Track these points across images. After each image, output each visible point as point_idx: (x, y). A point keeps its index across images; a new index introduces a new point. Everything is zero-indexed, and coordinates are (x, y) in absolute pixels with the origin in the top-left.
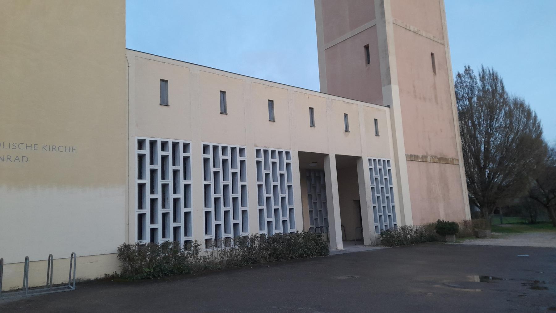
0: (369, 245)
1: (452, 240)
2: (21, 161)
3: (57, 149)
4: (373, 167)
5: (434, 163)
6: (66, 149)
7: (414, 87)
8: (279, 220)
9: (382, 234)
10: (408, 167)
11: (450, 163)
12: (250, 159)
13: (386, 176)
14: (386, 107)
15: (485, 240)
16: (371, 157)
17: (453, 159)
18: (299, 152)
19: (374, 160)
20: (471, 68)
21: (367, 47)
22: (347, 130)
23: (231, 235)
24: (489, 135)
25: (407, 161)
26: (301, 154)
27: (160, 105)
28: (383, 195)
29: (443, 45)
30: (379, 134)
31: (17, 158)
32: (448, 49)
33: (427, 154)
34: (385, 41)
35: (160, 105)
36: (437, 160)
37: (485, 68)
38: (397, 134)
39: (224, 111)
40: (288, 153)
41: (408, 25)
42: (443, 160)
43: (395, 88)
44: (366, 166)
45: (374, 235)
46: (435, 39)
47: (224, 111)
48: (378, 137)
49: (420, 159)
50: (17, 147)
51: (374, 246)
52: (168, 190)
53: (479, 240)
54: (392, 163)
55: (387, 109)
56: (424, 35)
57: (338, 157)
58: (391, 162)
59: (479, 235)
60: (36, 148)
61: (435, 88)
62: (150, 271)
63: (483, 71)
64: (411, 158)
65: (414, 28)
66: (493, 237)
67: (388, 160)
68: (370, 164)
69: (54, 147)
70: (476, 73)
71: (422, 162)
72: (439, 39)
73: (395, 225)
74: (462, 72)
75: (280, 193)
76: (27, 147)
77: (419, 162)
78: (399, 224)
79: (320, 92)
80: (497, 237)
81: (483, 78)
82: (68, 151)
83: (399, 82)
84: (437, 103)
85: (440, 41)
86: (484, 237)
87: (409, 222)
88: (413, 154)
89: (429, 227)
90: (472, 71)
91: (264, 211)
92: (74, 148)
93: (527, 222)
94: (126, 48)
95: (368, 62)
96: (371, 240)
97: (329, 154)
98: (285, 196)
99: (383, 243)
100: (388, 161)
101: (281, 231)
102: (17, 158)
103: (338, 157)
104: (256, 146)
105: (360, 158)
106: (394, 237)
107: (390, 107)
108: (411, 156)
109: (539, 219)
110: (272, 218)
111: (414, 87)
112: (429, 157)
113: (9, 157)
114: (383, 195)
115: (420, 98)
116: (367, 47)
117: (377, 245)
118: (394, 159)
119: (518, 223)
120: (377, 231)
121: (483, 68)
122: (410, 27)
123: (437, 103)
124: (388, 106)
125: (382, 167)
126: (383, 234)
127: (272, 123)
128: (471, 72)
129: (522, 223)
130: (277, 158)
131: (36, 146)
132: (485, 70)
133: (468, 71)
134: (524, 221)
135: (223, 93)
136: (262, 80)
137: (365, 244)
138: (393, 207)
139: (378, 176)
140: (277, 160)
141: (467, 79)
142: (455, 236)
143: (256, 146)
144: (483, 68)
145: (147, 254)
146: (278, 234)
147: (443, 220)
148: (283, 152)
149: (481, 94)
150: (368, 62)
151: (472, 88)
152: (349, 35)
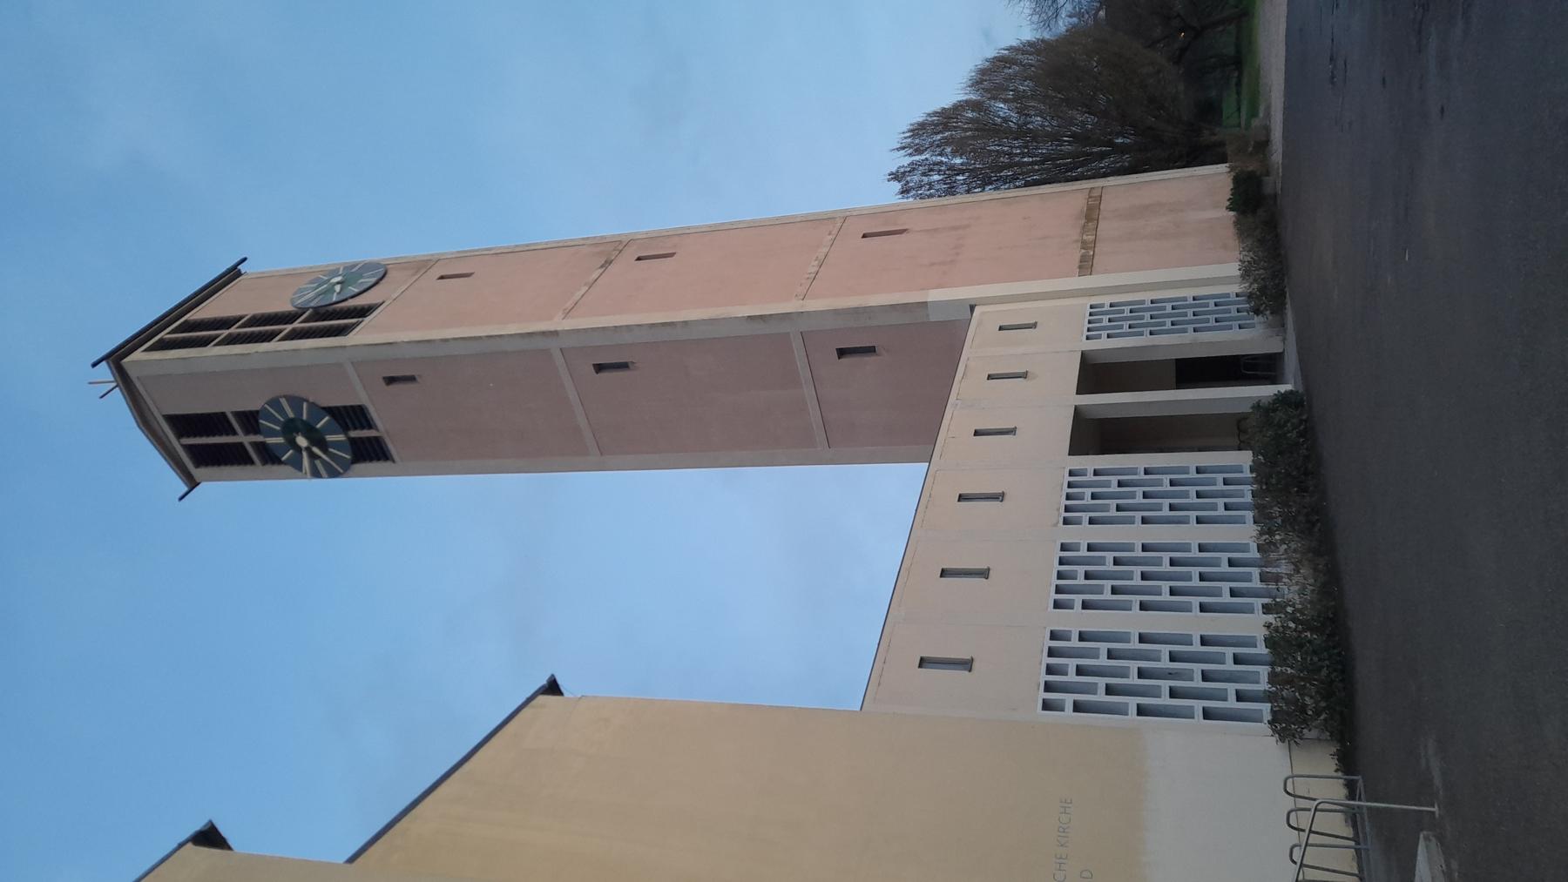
0: (1284, 340)
1: (1272, 184)
3: (1065, 826)
4: (1085, 516)
5: (1098, 229)
7: (933, 264)
8: (1222, 490)
9: (1257, 312)
10: (1106, 271)
11: (1098, 202)
12: (1075, 620)
14: (972, 314)
15: (1273, 126)
16: (1041, 664)
17: (1090, 197)
19: (1070, 485)
20: (894, 170)
21: (842, 353)
22: (1024, 375)
23: (1255, 572)
24: (1035, 136)
27: (970, 671)
28: (1169, 316)
29: (845, 219)
30: (1033, 321)
32: (854, 210)
33: (1077, 241)
34: (836, 312)
35: (970, 671)
36: (1090, 224)
37: (899, 146)
39: (984, 574)
40: (1054, 636)
42: (1091, 215)
43: (934, 295)
44: (1103, 344)
45: (1261, 331)
46: (835, 232)
47: (984, 574)
48: (991, 572)
51: (1285, 332)
52: (1147, 669)
53: (1272, 137)
54: (1095, 300)
55: (977, 310)
56: (825, 250)
57: (1081, 390)
58: (1092, 303)
59: (1264, 139)
61: (936, 230)
62: (1328, 666)
63: (903, 148)
64: (1086, 265)
65: (813, 266)
66: (1268, 115)
67: (1052, 605)
69: (1061, 830)
70: (904, 160)
71: (1096, 249)
72: (834, 227)
73: (1237, 295)
74: (897, 186)
75: (1158, 699)
78: (1235, 288)
79: (928, 464)
80: (1268, 108)
81: (919, 151)
82: (1063, 867)
83: (923, 289)
85: (839, 225)
86: (1267, 130)
87: (1233, 269)
88: (1077, 265)
89: (1242, 230)
90: (900, 167)
91: (1204, 573)
92: (1058, 856)
93: (1236, 74)
94: (858, 709)
95: (871, 350)
96: (1271, 336)
97: (1076, 406)
99: (1278, 310)
100: (1091, 307)
101: (1247, 489)
103: (1081, 390)
104: (1056, 525)
105: (1083, 354)
106: (1265, 287)
107: (973, 303)
108: (1080, 267)
109: (1231, 51)
110: (1226, 689)
112: (1085, 237)
114: (1169, 316)
115: (957, 254)
116: (842, 353)
117: (1283, 325)
118: (1087, 298)
119: (1238, 93)
120: (1252, 326)
121: (898, 149)
124: (972, 308)
125: (1081, 570)
126: (1258, 310)
127: (1006, 497)
128: (902, 170)
129: (1239, 84)
130: (1066, 663)
132: (903, 145)
133: (896, 176)
134: (1234, 81)
135: (923, 662)
136: (916, 510)
137: (1281, 351)
138: (1194, 299)
140: (1072, 663)
141: (915, 178)
142: (1266, 179)
143: (1056, 525)
144: (898, 149)
146: (1254, 494)
147: (1229, 200)
148: (1047, 679)
149: (949, 150)
150: (871, 350)
151: (931, 168)
152: (808, 392)
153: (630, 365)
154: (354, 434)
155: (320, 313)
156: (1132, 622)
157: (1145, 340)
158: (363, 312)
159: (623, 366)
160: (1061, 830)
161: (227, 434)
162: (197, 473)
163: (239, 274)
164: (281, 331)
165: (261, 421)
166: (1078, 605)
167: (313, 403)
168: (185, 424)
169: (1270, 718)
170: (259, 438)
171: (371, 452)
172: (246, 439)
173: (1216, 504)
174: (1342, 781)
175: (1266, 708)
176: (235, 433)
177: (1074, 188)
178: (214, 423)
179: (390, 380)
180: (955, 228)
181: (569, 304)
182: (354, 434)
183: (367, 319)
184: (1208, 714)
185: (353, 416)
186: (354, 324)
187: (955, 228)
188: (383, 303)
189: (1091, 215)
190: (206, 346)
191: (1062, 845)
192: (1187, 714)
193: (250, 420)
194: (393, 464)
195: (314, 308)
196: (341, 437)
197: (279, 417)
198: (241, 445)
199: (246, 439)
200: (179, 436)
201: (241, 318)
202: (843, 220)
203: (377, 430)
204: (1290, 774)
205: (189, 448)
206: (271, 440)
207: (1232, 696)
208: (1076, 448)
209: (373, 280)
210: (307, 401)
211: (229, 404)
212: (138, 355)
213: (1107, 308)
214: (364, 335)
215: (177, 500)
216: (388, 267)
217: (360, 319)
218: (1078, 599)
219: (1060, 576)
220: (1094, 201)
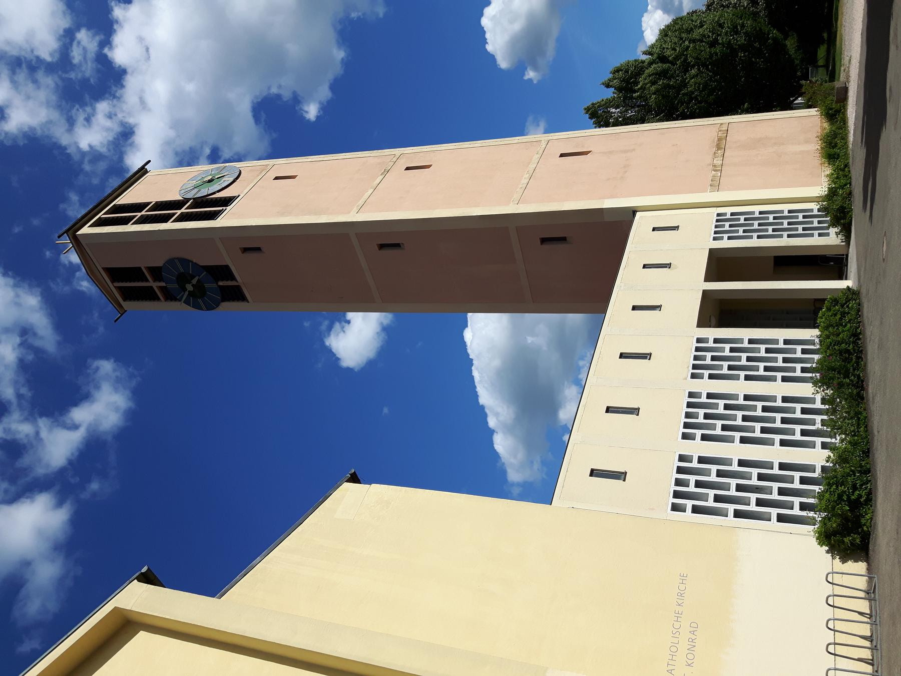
2: (696, 629)
6: (672, 660)
7: (608, 179)
10: (729, 189)
12: (698, 448)
13: (705, 375)
18: (697, 327)
25: (724, 190)
26: (702, 323)
31: (693, 632)
36: (719, 151)
38: (105, 279)
41: (521, 186)
42: (720, 144)
44: (725, 243)
46: (541, 152)
49: (718, 174)
50: (677, 630)
55: (638, 214)
57: (708, 279)
60: (680, 613)
61: (611, 152)
64: (716, 185)
68: (722, 238)
76: (673, 659)
77: (722, 175)
83: (600, 199)
84: (634, 150)
86: (846, 90)
95: (563, 239)
98: (777, 489)
102: (693, 633)
103: (708, 279)
104: (686, 379)
111: (608, 179)
112: (715, 162)
113: (690, 640)
122: (523, 184)
123: (634, 150)
131: (677, 612)
135: (608, 410)
139: (697, 433)
143: (686, 379)
145: (840, 513)
150: (563, 239)
153: (401, 245)
154: (221, 283)
155: (199, 202)
156: (735, 451)
157: (754, 242)
158: (227, 201)
159: (397, 246)
160: (679, 594)
161: (142, 281)
162: (126, 305)
163: (146, 172)
164: (174, 214)
165: (163, 273)
166: (698, 437)
167: (195, 263)
168: (116, 274)
169: (830, 439)
170: (163, 284)
171: (236, 294)
172: (155, 285)
173: (793, 477)
174: (867, 578)
175: (818, 517)
176: (147, 280)
177: (710, 123)
178: (134, 273)
179: (245, 250)
180: (625, 152)
181: (361, 202)
182: (221, 283)
183: (229, 208)
184: (781, 518)
185: (223, 272)
186: (220, 211)
187: (625, 152)
188: (239, 196)
189: (720, 144)
190: (127, 224)
191: (679, 605)
192: (767, 518)
193: (156, 272)
194: (247, 303)
195: (194, 199)
196: (214, 285)
197: (191, 300)
198: (151, 287)
199: (155, 285)
200: (112, 282)
201: (149, 204)
202: (547, 143)
203: (236, 281)
204: (831, 593)
205: (119, 289)
206: (169, 286)
207: (797, 506)
208: (703, 322)
209: (231, 179)
210: (192, 262)
211: (143, 262)
212: (86, 230)
213: (728, 216)
214: (228, 219)
215: (114, 322)
216: (241, 169)
217: (224, 208)
218: (699, 433)
219: (688, 415)
220: (723, 134)
